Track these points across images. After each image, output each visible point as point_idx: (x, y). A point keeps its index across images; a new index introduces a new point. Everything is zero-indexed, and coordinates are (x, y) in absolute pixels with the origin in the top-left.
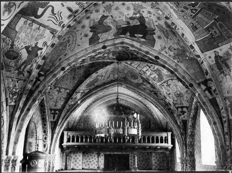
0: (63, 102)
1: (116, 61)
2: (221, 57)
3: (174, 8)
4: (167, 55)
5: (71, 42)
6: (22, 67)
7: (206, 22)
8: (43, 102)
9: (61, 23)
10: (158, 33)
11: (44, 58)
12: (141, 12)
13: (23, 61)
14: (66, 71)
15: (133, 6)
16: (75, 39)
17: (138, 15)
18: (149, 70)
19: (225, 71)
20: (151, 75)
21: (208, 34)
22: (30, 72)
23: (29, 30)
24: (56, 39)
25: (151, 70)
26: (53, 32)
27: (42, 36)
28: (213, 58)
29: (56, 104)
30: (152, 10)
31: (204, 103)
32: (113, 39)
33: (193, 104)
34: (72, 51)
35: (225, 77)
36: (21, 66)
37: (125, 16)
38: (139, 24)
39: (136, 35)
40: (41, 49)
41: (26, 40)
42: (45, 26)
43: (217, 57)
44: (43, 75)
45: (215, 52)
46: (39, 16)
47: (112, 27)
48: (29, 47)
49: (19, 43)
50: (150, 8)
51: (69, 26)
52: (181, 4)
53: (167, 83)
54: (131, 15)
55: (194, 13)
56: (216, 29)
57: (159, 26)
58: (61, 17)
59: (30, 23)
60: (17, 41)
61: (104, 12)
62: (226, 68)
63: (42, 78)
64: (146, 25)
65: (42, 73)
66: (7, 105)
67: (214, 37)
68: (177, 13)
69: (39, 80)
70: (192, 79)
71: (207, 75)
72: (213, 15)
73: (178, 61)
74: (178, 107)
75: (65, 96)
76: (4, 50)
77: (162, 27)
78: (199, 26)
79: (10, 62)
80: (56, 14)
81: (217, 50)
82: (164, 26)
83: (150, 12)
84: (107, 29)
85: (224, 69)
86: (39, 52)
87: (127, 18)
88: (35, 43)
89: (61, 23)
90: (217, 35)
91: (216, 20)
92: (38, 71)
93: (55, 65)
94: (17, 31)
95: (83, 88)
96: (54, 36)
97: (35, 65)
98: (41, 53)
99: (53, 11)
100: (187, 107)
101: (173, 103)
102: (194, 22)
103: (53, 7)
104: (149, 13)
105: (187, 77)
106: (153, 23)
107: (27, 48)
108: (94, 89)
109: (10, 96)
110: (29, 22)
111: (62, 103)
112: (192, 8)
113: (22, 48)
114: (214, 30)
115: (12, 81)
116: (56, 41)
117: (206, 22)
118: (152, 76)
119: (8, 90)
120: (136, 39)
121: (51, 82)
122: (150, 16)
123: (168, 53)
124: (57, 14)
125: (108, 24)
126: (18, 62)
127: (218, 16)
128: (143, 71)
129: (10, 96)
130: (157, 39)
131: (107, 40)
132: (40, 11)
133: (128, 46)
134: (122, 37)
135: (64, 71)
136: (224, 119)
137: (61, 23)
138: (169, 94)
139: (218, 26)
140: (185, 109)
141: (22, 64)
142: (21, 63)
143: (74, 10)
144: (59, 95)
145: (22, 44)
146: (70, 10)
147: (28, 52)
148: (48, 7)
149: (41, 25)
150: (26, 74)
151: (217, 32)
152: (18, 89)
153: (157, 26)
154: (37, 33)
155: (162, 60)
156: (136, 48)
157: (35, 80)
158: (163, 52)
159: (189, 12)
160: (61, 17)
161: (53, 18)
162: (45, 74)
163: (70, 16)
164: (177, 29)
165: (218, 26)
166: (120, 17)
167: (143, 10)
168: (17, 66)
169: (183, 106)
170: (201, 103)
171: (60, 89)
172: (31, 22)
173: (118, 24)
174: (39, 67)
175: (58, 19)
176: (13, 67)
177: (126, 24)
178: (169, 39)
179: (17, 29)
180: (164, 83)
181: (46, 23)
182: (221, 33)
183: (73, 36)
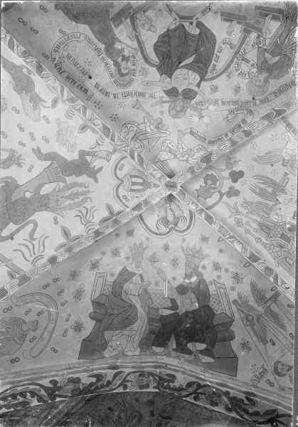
3: (264, 240)
10: (240, 332)
15: (185, 255)
16: (51, 327)
17: (194, 279)
34: (34, 357)
37: (169, 282)
38: (197, 304)
39: (190, 345)
54: (180, 281)
58: (44, 246)
61: (128, 258)
68: (271, 251)
77: (246, 303)
80: (35, 240)
82: (252, 302)
83: (218, 263)
87: (172, 287)
99: (33, 231)
104: (217, 267)
106: (227, 295)
116: (12, 287)
122: (219, 277)
124: (38, 240)
130: (241, 354)
143: (74, 234)
146: (66, 233)
153: (235, 302)
158: (262, 384)
160: (44, 246)
161: (27, 246)
164: (279, 283)
173: (153, 303)
178: (269, 344)
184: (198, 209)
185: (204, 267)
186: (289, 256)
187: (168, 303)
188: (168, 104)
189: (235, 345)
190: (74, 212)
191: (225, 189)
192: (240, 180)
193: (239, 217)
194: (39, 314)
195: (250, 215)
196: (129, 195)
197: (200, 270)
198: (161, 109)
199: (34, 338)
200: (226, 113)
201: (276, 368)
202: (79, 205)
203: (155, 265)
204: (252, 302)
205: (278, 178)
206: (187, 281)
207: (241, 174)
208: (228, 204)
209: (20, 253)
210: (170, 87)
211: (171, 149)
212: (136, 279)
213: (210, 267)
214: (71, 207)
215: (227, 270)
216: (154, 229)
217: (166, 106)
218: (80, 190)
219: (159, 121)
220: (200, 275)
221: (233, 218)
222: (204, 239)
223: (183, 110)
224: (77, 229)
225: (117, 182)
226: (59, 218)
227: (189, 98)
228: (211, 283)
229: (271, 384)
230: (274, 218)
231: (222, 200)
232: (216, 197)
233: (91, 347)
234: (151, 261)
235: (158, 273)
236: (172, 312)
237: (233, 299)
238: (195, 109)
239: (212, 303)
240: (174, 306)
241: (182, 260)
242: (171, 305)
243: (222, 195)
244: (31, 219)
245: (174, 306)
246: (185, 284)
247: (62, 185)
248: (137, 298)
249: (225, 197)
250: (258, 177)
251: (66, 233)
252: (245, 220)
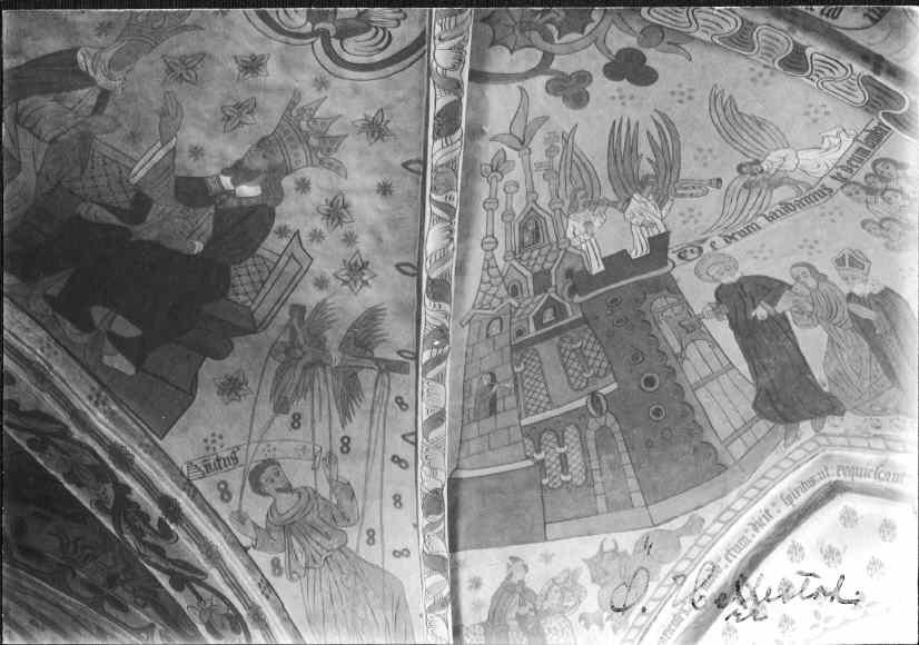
3: (499, 253)
7: (548, 395)
9: (382, 45)
17: (249, 190)
21: (527, 458)
38: (199, 247)
39: (98, 313)
45: (515, 559)
52: (545, 251)
54: (209, 169)
64: (236, 281)
67: (545, 481)
72: (602, 373)
73: (275, 564)
78: (511, 401)
81: (531, 553)
83: (345, 206)
90: (568, 478)
91: (598, 400)
102: (504, 372)
104: (336, 211)
106: (293, 284)
114: (563, 450)
117: (548, 395)
122: (316, 236)
123: (235, 498)
137: (382, 45)
139: (591, 435)
153: (299, 309)
165: (591, 435)
177: (113, 210)
178: (286, 419)
184: (450, 74)
185: (303, 186)
186: (506, 319)
187: (122, 197)
191: (564, 64)
192: (625, 83)
193: (511, 154)
195: (538, 177)
197: (288, 183)
201: (259, 470)
203: (174, 87)
205: (689, 169)
206: (226, 181)
212: (86, 96)
213: (316, 197)
215: (350, 239)
220: (273, 191)
221: (498, 145)
222: (375, 129)
228: (282, 232)
229: (225, 494)
230: (574, 226)
231: (527, 84)
232: (526, 59)
234: (170, 70)
235: (163, 114)
237: (303, 302)
239: (243, 271)
240: (141, 203)
241: (266, 121)
242: (127, 206)
246: (214, 187)
250: (666, 125)
252: (516, 174)
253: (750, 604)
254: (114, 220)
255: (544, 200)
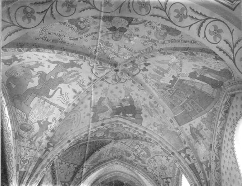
0: (72, 175)
1: (113, 140)
2: (195, 129)
3: (156, 89)
4: (152, 130)
5: (76, 120)
6: (34, 138)
8: (55, 175)
10: (144, 112)
11: (53, 131)
12: (130, 94)
13: (35, 133)
14: (72, 143)
17: (128, 97)
18: (140, 148)
19: (199, 140)
20: (141, 152)
21: (183, 110)
22: (40, 143)
23: (42, 107)
24: (63, 115)
25: (141, 148)
26: (61, 109)
27: (52, 112)
28: (189, 130)
29: (66, 177)
30: (139, 93)
31: (185, 168)
32: (109, 118)
33: (175, 175)
35: (200, 145)
36: (33, 138)
39: (127, 115)
40: (51, 123)
41: (39, 115)
42: (55, 105)
43: (192, 129)
44: (52, 147)
45: (190, 124)
46: (50, 96)
47: (109, 107)
48: (41, 121)
49: (33, 117)
50: (137, 90)
51: (74, 104)
53: (154, 159)
55: (171, 93)
56: (189, 106)
57: (145, 106)
59: (43, 102)
60: (31, 117)
62: (200, 137)
63: (50, 149)
65: (51, 144)
66: (17, 171)
69: (48, 150)
70: (173, 148)
71: (185, 144)
74: (163, 179)
75: (73, 170)
76: (19, 123)
79: (24, 134)
80: (63, 95)
81: (192, 122)
82: (149, 106)
84: (105, 110)
85: (198, 139)
86: (49, 126)
87: (120, 100)
88: (46, 118)
89: (68, 103)
92: (47, 142)
93: (62, 138)
94: (31, 108)
95: (87, 164)
96: (62, 113)
97: (45, 137)
98: (51, 127)
100: (170, 178)
101: (160, 175)
102: (171, 101)
103: (61, 89)
104: (137, 95)
105: (170, 148)
107: (39, 122)
108: (97, 165)
109: (21, 164)
110: (42, 101)
111: (71, 177)
112: (170, 89)
113: (35, 122)
115: (24, 150)
118: (142, 153)
119: (20, 157)
120: (127, 118)
121: (59, 152)
125: (105, 105)
126: (30, 134)
127: (189, 95)
128: (135, 149)
129: (21, 164)
130: (144, 118)
131: (105, 119)
132: (51, 92)
133: (122, 124)
134: (117, 117)
135: (69, 143)
136: (203, 181)
138: (156, 168)
140: (169, 180)
141: (35, 135)
142: (34, 135)
143: (78, 91)
144: (69, 169)
145: (35, 118)
146: (75, 91)
147: (40, 125)
148: (58, 88)
149: (51, 103)
150: (37, 144)
151: (191, 108)
152: (29, 157)
153: (143, 106)
154: (48, 110)
155: (149, 134)
156: (128, 125)
157: (44, 150)
159: (167, 92)
162: (54, 145)
163: (75, 97)
165: (190, 103)
166: (114, 99)
167: (132, 92)
168: (29, 137)
169: (167, 177)
170: (182, 168)
171: (69, 165)
172: (44, 101)
174: (48, 138)
175: (66, 99)
176: (26, 138)
178: (153, 117)
179: (32, 106)
180: (151, 158)
181: (56, 103)
182: (193, 108)
183: (78, 114)
188: (112, 35)
189: (142, 115)
190: (75, 83)
191: (142, 68)
193: (147, 79)
194: (74, 115)
195: (152, 79)
196: (98, 72)
198: (107, 37)
199: (75, 122)
200: (143, 42)
202: (76, 79)
204: (149, 106)
207: (149, 64)
208: (143, 75)
209: (60, 101)
210: (111, 26)
211: (115, 53)
214: (73, 81)
216: (112, 83)
217: (110, 36)
218: (75, 73)
219: (107, 42)
223: (120, 37)
224: (79, 89)
225: (90, 68)
226: (70, 86)
227: (123, 32)
230: (161, 81)
233: (95, 119)
236: (121, 106)
238: (127, 37)
240: (121, 104)
241: (123, 91)
243: (140, 70)
244: (58, 87)
245: (121, 104)
247: (66, 72)
248: (108, 105)
249: (141, 71)
251: (75, 91)
252: (149, 81)
253: (205, 135)
254: (120, 106)
255: (155, 81)
